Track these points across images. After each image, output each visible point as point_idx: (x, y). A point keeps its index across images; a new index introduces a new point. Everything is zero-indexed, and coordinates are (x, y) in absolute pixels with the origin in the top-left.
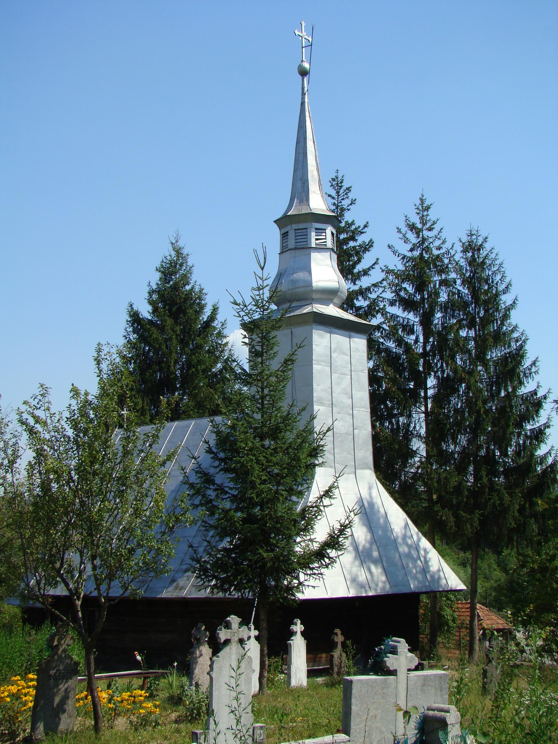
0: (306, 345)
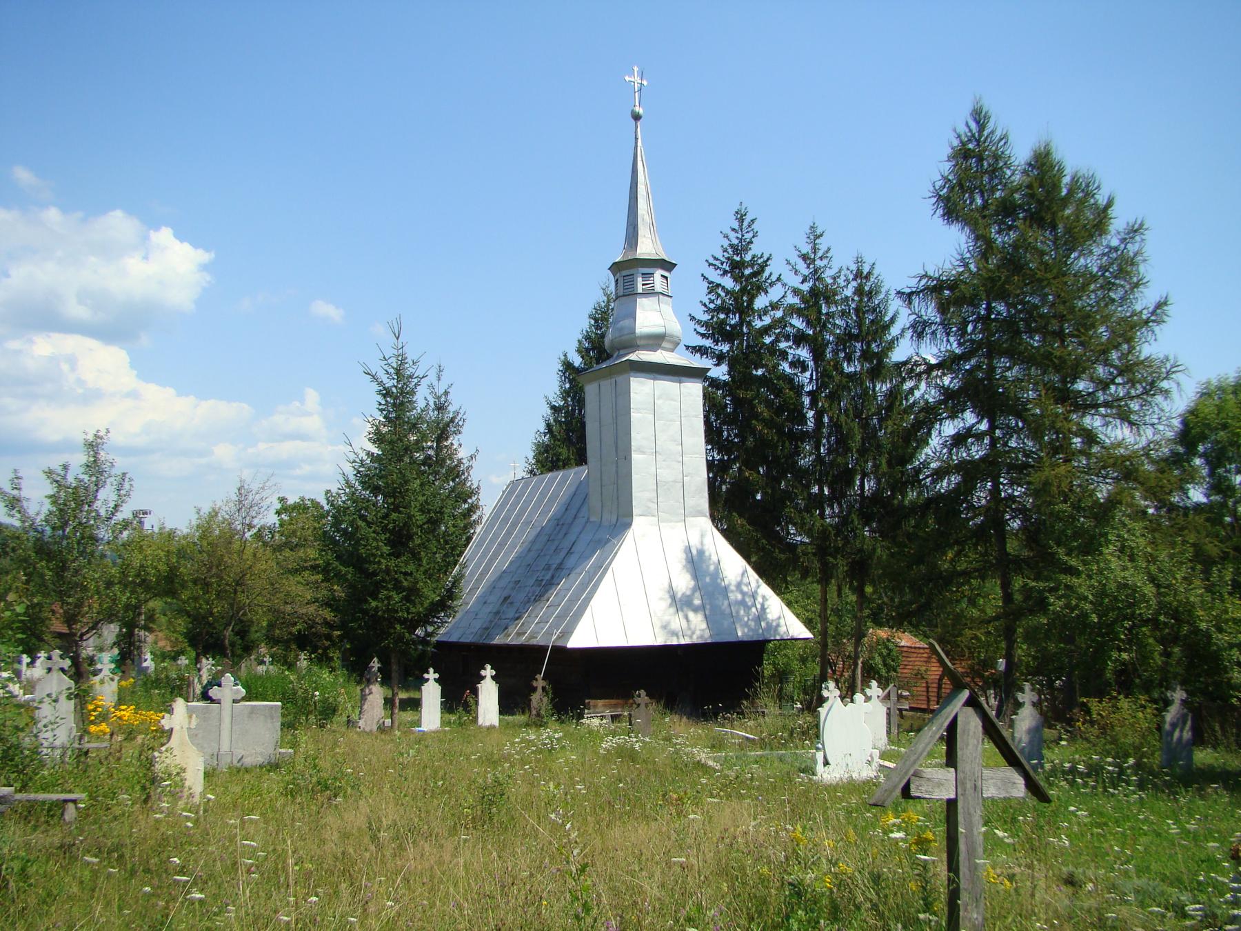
0: (623, 397)
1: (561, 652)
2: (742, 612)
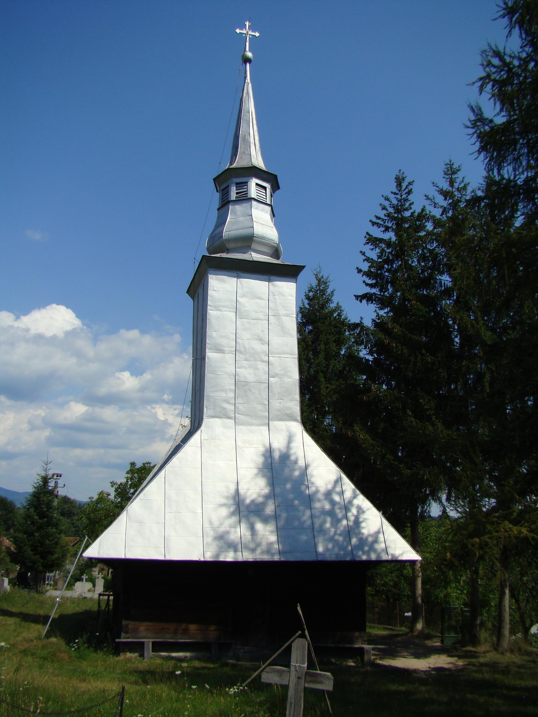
2: (328, 525)
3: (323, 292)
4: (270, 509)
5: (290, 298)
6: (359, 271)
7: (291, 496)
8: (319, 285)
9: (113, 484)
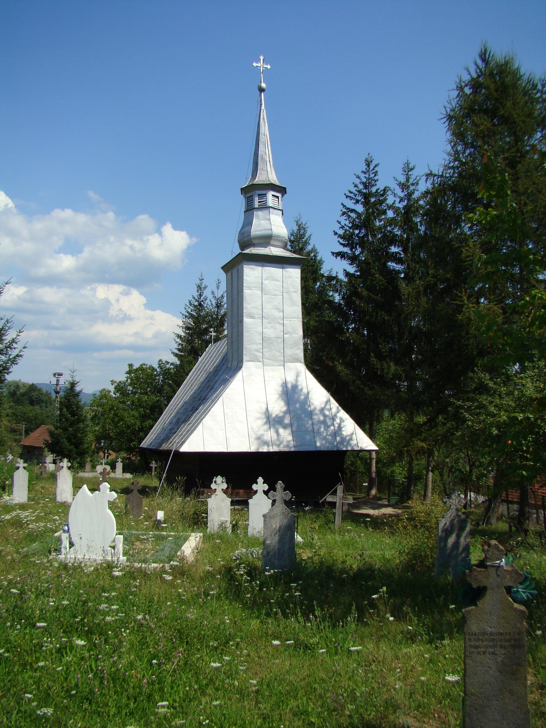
1: (179, 455)
2: (322, 429)
3: (302, 236)
4: (287, 421)
5: (297, 280)
6: (336, 234)
7: (299, 412)
8: (299, 230)
9: (113, 382)
